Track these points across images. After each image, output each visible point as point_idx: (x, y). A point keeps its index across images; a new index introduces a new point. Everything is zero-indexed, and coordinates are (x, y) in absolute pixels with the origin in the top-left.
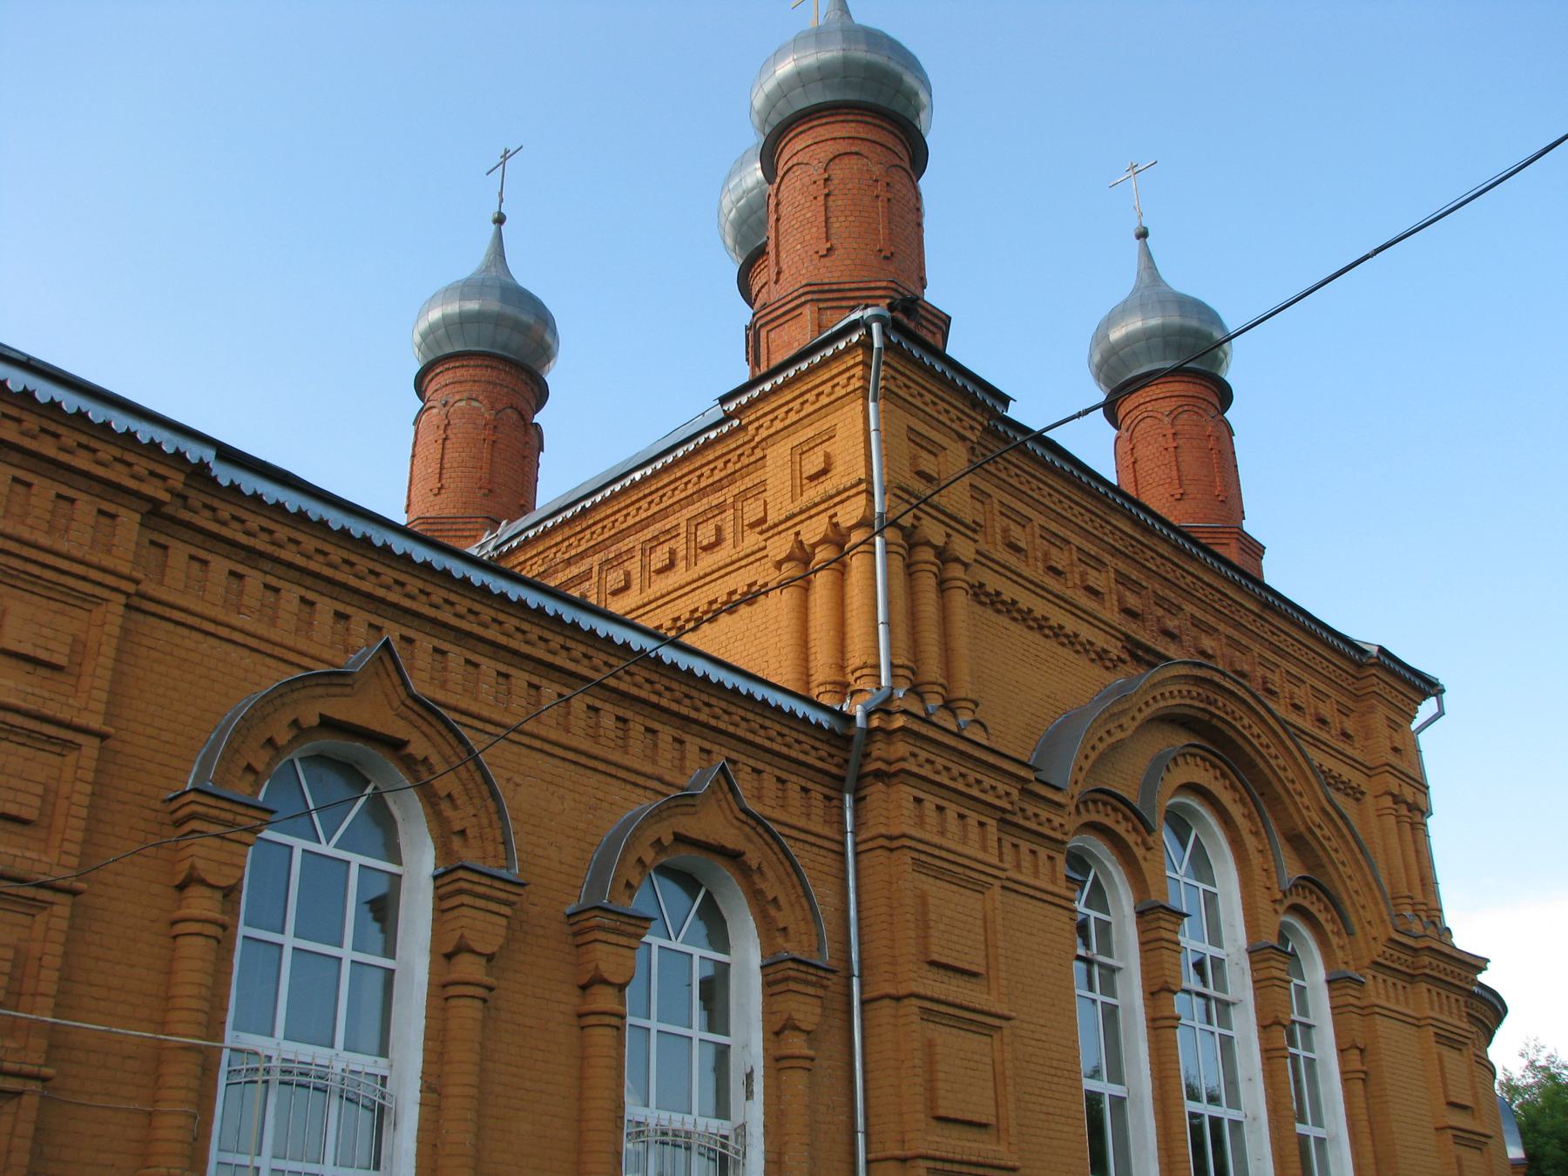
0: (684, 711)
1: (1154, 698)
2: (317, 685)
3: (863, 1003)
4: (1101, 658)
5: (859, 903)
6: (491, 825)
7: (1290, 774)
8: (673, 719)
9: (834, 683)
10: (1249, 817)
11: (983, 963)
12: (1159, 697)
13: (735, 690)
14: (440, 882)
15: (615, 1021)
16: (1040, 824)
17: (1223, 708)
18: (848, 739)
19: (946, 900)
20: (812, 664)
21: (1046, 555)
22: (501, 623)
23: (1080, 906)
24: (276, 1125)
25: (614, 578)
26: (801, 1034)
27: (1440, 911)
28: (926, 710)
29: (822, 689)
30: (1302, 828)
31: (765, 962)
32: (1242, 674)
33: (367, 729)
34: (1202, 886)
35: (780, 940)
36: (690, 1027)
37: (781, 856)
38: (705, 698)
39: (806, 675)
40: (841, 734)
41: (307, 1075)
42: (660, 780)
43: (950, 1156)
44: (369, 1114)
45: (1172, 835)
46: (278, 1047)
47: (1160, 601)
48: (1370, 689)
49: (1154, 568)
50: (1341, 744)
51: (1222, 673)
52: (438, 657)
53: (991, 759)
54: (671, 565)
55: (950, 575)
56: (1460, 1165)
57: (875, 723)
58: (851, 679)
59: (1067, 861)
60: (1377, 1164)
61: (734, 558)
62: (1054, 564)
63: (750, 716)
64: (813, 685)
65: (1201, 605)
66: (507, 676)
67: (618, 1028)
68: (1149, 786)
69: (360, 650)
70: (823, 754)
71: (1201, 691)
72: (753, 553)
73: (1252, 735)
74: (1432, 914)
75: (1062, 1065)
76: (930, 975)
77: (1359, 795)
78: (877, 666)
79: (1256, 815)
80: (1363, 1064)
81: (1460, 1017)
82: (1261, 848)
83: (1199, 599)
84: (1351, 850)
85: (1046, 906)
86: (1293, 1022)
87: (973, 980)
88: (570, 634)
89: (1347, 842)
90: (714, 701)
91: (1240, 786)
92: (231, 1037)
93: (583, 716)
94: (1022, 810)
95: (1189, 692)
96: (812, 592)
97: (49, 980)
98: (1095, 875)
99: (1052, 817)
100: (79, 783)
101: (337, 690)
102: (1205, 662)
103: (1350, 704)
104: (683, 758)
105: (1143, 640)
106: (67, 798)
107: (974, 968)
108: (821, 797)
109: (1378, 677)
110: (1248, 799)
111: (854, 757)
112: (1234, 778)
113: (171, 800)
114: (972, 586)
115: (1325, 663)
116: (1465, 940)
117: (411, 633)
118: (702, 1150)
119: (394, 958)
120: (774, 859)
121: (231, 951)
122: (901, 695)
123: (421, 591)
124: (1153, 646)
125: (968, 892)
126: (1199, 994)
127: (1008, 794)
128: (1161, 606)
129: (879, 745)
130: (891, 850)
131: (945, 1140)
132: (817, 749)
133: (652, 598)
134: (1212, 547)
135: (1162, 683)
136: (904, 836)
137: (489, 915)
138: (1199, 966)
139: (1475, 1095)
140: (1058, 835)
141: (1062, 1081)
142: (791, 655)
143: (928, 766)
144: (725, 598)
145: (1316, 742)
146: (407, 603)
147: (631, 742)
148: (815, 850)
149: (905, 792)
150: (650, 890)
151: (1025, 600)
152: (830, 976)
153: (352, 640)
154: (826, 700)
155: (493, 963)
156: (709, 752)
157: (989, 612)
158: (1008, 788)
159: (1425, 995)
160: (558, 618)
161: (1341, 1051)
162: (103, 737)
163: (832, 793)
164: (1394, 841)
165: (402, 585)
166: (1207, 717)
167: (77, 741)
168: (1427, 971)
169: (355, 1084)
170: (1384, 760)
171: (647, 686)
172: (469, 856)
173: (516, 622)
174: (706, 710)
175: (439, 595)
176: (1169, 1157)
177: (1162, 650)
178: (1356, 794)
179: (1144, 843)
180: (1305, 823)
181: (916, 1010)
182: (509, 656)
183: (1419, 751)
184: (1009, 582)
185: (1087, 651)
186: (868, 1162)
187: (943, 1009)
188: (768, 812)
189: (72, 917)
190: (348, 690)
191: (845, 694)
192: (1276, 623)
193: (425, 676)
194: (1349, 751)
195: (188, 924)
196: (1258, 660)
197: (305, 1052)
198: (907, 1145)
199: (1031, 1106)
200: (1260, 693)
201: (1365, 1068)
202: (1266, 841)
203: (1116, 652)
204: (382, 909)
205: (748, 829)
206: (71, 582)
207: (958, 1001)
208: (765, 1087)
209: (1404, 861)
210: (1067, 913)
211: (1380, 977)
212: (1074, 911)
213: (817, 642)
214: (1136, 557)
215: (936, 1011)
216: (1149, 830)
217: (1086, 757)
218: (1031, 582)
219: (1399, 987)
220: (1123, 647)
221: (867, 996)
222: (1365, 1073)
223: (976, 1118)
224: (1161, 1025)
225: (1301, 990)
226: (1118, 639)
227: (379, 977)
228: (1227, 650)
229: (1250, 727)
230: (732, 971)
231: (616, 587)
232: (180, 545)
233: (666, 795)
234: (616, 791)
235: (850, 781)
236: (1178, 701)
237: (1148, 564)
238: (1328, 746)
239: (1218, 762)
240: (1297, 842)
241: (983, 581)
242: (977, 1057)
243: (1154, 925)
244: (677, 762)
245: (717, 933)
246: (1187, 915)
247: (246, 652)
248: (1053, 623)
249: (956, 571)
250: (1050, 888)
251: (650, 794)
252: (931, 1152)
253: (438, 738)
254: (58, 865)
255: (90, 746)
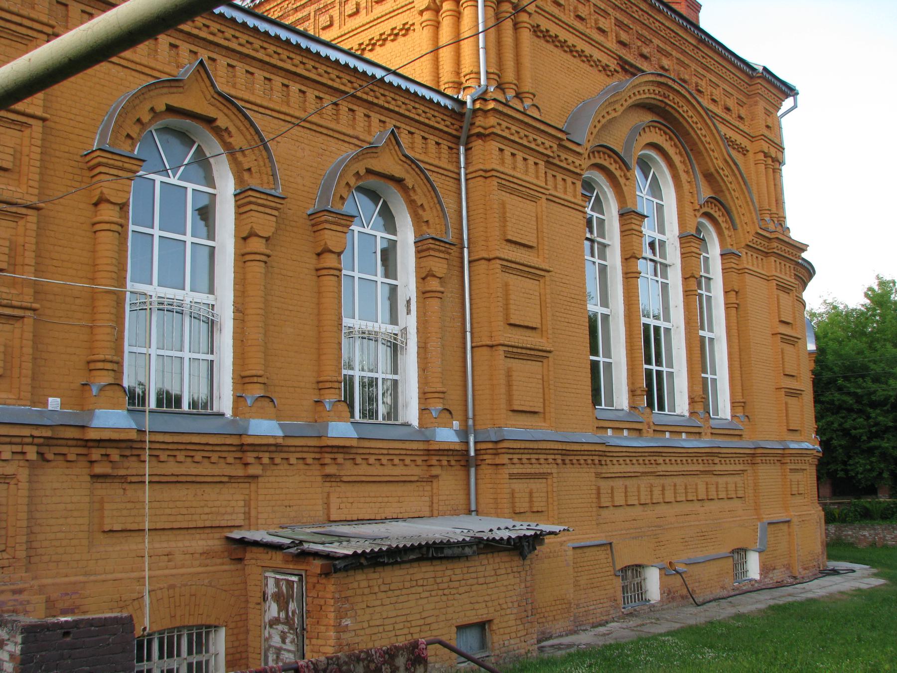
0: (370, 99)
1: (634, 94)
2: (163, 87)
3: (470, 262)
4: (605, 70)
5: (468, 207)
6: (265, 165)
7: (708, 139)
8: (365, 103)
9: (453, 82)
10: (684, 162)
11: (536, 241)
12: (637, 93)
13: (399, 87)
14: (238, 198)
15: (336, 273)
16: (568, 164)
17: (673, 100)
18: (462, 115)
19: (518, 208)
20: (441, 71)
21: (575, 8)
22: (265, 49)
23: (588, 210)
24: (158, 331)
25: (324, 20)
26: (436, 279)
27: (785, 218)
28: (506, 99)
29: (447, 86)
30: (712, 170)
31: (417, 240)
32: (684, 81)
33: (192, 112)
34: (655, 201)
35: (425, 228)
36: (376, 275)
37: (425, 181)
38: (382, 91)
39: (437, 77)
40: (458, 113)
41: (171, 305)
42: (358, 138)
43: (517, 344)
44: (206, 325)
45: (640, 171)
46: (155, 290)
47: (640, 37)
48: (756, 92)
49: (637, 17)
50: (737, 123)
51: (674, 81)
52: (230, 69)
53: (542, 127)
54: (357, 12)
55: (520, 19)
56: (782, 353)
57: (478, 106)
58: (463, 80)
59: (582, 186)
60: (740, 352)
61: (395, 8)
62: (580, 14)
63: (407, 101)
64: (441, 83)
65: (663, 39)
66: (270, 80)
67: (338, 276)
68: (629, 144)
69: (186, 68)
70: (448, 123)
71: (660, 90)
72: (406, 5)
73: (688, 116)
74: (780, 220)
75: (576, 297)
76: (507, 247)
77: (745, 152)
78: (479, 73)
79: (687, 161)
80: (737, 299)
81: (790, 276)
82: (689, 180)
83: (662, 36)
84: (739, 183)
85: (570, 210)
86: (701, 276)
87: (530, 250)
88: (305, 55)
89: (737, 178)
90: (387, 93)
91: (679, 145)
92: (130, 286)
93: (314, 102)
94: (559, 156)
95: (654, 90)
96: (440, 29)
97: (30, 257)
98: (597, 193)
99: (575, 160)
100: (33, 147)
101: (175, 90)
102: (664, 73)
103: (744, 100)
104: (370, 126)
105: (629, 60)
106: (28, 156)
107: (530, 244)
108: (447, 148)
109: (762, 85)
110: (684, 153)
111: (465, 125)
112: (676, 140)
113: (86, 155)
114: (533, 27)
115: (732, 76)
116: (796, 235)
117: (214, 56)
118: (384, 342)
119: (214, 241)
120: (422, 182)
121: (126, 239)
122: (492, 90)
123: (219, 30)
124: (635, 63)
125: (528, 202)
126: (651, 260)
127: (551, 147)
128: (640, 40)
129: (480, 118)
130: (486, 178)
131: (513, 336)
132: (444, 121)
133: (346, 31)
134: (671, 5)
135: (639, 85)
136: (493, 170)
137: (266, 216)
138: (652, 245)
139: (794, 318)
140: (578, 171)
141: (577, 305)
142: (429, 66)
143: (507, 131)
144: (389, 32)
145: (724, 121)
146: (211, 38)
147: (341, 117)
148: (443, 177)
149: (494, 146)
150: (353, 204)
151: (563, 35)
152: (452, 247)
153: (181, 60)
154: (449, 92)
155: (269, 242)
156: (384, 122)
157: (542, 41)
158: (552, 144)
159: (773, 263)
160: (298, 46)
161: (726, 292)
162: (44, 120)
163: (453, 146)
164: (763, 179)
165: (208, 27)
166: (663, 105)
167: (30, 123)
168: (775, 251)
169: (198, 309)
170: (761, 133)
171: (349, 85)
172: (254, 183)
173: (274, 48)
174: (383, 98)
175: (229, 32)
176: (631, 346)
177: (640, 66)
178: (744, 151)
179: (625, 176)
180: (714, 167)
181: (499, 267)
182: (270, 68)
183: (780, 128)
184: (554, 25)
185: (597, 66)
186: (472, 347)
187: (514, 266)
188: (418, 156)
189: (38, 222)
190: (181, 90)
191: (460, 89)
192: (705, 52)
193: (224, 80)
194: (741, 127)
195: (101, 225)
196: (693, 73)
197: (170, 293)
198: (493, 339)
199: (560, 318)
200: (694, 92)
201: (737, 302)
202: (692, 176)
203: (613, 66)
204: (206, 214)
205: (406, 166)
206: (13, 27)
207: (521, 262)
208: (417, 307)
209: (768, 190)
210: (581, 214)
211: (750, 253)
212: (585, 213)
213: (444, 58)
214: (627, 10)
215: (509, 267)
216: (628, 168)
217: (595, 127)
218: (567, 24)
219: (760, 259)
220: (618, 64)
221: (472, 258)
222: (738, 304)
223: (530, 325)
224: (630, 276)
225: (706, 259)
226: (615, 59)
227: (207, 250)
228: (676, 67)
229: (687, 111)
230: (398, 244)
231: (325, 25)
232: (75, 4)
233: (361, 147)
234: (333, 145)
235: (463, 139)
236: (647, 95)
237: (634, 15)
238: (730, 124)
239: (668, 131)
240: (709, 177)
241: (539, 23)
242: (531, 292)
243: (629, 221)
244: (366, 128)
245: (390, 224)
246: (647, 217)
247: (120, 69)
248: (579, 49)
249: (524, 17)
250: (573, 200)
251: (352, 146)
252: (506, 343)
253: (233, 117)
254: (27, 193)
255: (37, 125)
